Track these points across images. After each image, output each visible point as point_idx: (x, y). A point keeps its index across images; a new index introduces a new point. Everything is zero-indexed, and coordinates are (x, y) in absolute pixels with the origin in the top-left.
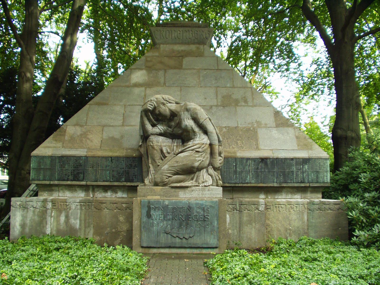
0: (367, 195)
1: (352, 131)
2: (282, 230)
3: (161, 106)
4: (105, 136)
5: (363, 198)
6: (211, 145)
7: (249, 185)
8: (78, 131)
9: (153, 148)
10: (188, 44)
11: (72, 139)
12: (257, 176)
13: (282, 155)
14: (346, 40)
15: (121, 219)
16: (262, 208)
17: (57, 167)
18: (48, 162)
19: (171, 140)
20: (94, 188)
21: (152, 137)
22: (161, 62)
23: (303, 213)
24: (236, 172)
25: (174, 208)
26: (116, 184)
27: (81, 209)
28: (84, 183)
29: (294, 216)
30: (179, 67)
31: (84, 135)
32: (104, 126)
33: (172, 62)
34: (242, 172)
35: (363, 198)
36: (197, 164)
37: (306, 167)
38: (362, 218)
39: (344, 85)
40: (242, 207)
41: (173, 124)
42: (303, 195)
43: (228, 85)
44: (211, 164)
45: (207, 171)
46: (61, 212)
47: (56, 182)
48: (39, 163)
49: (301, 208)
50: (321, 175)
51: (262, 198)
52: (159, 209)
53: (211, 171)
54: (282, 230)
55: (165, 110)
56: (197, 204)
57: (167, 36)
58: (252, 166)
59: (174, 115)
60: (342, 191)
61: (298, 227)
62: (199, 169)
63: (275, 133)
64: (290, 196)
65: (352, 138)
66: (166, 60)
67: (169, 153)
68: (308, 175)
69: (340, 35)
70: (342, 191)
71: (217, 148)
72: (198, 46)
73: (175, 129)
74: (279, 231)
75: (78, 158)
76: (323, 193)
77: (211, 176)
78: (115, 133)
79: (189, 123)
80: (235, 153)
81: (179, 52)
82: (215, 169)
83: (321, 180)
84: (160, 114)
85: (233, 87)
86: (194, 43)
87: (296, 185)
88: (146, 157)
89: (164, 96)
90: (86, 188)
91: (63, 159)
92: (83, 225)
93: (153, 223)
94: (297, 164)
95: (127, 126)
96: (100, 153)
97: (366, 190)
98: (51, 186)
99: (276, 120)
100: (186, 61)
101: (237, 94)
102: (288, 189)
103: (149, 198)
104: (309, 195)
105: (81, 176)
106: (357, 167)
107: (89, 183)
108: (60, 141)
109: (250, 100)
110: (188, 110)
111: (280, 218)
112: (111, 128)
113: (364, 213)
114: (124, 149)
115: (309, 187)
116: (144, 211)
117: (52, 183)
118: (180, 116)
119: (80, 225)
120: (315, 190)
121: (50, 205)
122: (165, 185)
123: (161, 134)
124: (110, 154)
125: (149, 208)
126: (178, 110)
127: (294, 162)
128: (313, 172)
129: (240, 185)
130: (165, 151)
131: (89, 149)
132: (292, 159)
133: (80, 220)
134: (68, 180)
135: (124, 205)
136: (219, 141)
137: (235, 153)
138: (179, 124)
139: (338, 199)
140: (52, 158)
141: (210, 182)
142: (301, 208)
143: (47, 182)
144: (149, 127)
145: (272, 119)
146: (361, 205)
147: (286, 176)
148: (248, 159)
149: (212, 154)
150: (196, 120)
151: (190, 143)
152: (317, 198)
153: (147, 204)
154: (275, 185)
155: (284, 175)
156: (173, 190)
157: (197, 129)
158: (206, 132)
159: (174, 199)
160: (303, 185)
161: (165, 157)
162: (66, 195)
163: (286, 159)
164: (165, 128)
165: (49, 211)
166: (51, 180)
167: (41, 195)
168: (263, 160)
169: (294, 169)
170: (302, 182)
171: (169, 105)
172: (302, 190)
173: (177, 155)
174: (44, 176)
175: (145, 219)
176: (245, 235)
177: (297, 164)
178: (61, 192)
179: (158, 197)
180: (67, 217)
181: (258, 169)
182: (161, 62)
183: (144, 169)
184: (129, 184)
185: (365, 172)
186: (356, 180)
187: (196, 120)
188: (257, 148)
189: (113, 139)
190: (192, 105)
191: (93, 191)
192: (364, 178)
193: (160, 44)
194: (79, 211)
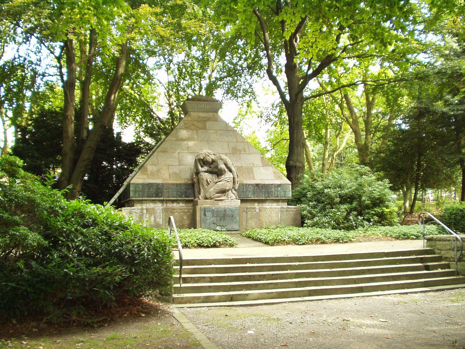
0: (311, 203)
1: (300, 162)
2: (268, 221)
3: (207, 157)
4: (171, 171)
5: (309, 205)
6: (234, 178)
7: (250, 198)
8: (155, 168)
9: (203, 179)
10: (208, 112)
11: (152, 174)
12: (254, 193)
13: (267, 182)
14: (298, 102)
15: (185, 217)
16: (257, 211)
17: (147, 190)
18: (141, 187)
19: (211, 175)
20: (167, 201)
21: (201, 173)
22: (194, 125)
23: (278, 213)
24: (243, 192)
25: (217, 211)
26: (180, 199)
27: (163, 213)
28: (162, 198)
29: (274, 215)
30: (204, 128)
31: (158, 171)
32: (169, 165)
33: (200, 125)
34: (246, 191)
35: (309, 205)
36: (227, 188)
37: (279, 189)
38: (308, 214)
39: (295, 131)
40: (248, 210)
41: (212, 166)
42: (277, 204)
43: (234, 141)
44: (233, 188)
45: (232, 191)
46: (151, 215)
47: (146, 198)
48: (135, 188)
49: (277, 210)
50: (287, 193)
51: (256, 205)
52: (210, 211)
53: (234, 191)
54: (268, 221)
55: (209, 159)
56: (228, 208)
57: (195, 107)
58: (252, 188)
59: (213, 161)
60: (297, 202)
61: (276, 221)
62: (228, 191)
63: (262, 170)
64: (270, 204)
65: (300, 167)
66: (196, 123)
67: (211, 182)
68: (280, 193)
69: (294, 97)
70: (297, 202)
71: (236, 179)
72: (213, 113)
73: (214, 169)
74: (266, 222)
75: (158, 185)
76: (288, 202)
77: (234, 194)
78: (176, 170)
79: (223, 166)
80: (242, 181)
81: (203, 118)
82: (235, 190)
83: (287, 196)
84: (207, 161)
85: (237, 142)
86: (211, 112)
87: (274, 198)
88: (197, 184)
89: (208, 151)
90: (162, 201)
91: (150, 185)
92: (164, 222)
93: (207, 219)
94: (275, 187)
95: (182, 165)
96: (170, 182)
97: (310, 201)
98: (142, 200)
99: (262, 163)
100: (208, 124)
101: (240, 147)
102: (270, 201)
103: (204, 206)
104: (280, 203)
105: (160, 194)
106: (305, 189)
107: (165, 199)
108: (145, 174)
109: (247, 150)
110: (222, 159)
111: (267, 216)
112: (173, 167)
113: (310, 212)
114: (183, 179)
115: (281, 199)
116: (203, 213)
117: (143, 199)
118: (217, 162)
119: (163, 222)
120: (283, 201)
121: (145, 211)
122: (211, 199)
123: (205, 172)
124: (176, 182)
125: (205, 210)
126: (216, 159)
127: (273, 186)
128: (282, 192)
129: (245, 198)
130: (209, 181)
131: (163, 179)
132: (272, 185)
133: (162, 219)
134: (152, 197)
135: (186, 210)
136: (237, 176)
137: (242, 181)
138: (217, 167)
139: (296, 206)
140: (143, 185)
141: (234, 197)
142: (277, 210)
143: (141, 199)
144: (200, 167)
145: (260, 162)
146: (308, 208)
147: (269, 193)
148: (249, 185)
149: (234, 182)
150: (226, 165)
151: (223, 176)
152: (285, 205)
153: (204, 209)
154: (264, 198)
155: (268, 193)
156: (216, 201)
157: (226, 170)
158: (231, 171)
159: (217, 206)
160: (277, 198)
161: (209, 184)
162: (151, 205)
163: (269, 184)
164: (208, 168)
165: (145, 215)
166: (143, 197)
167: (136, 206)
168: (257, 185)
169: (273, 190)
170: (277, 197)
171: (211, 156)
172: (277, 201)
173: (216, 183)
174: (139, 195)
175: (203, 217)
176: (249, 225)
177: (275, 187)
178: (148, 203)
179: (208, 205)
180: (155, 217)
181: (254, 189)
182: (194, 125)
183: (196, 190)
184: (187, 199)
185: (310, 192)
186: (305, 196)
187: (226, 165)
188: (254, 179)
189: (175, 173)
190: (224, 157)
191: (166, 203)
192: (309, 195)
193: (190, 112)
194: (162, 214)
